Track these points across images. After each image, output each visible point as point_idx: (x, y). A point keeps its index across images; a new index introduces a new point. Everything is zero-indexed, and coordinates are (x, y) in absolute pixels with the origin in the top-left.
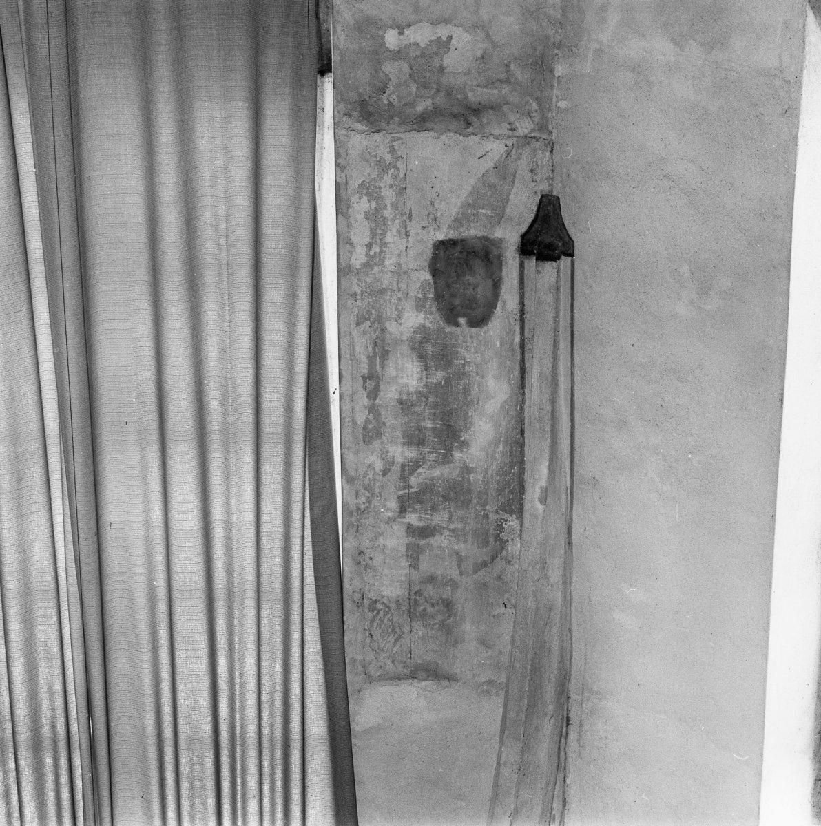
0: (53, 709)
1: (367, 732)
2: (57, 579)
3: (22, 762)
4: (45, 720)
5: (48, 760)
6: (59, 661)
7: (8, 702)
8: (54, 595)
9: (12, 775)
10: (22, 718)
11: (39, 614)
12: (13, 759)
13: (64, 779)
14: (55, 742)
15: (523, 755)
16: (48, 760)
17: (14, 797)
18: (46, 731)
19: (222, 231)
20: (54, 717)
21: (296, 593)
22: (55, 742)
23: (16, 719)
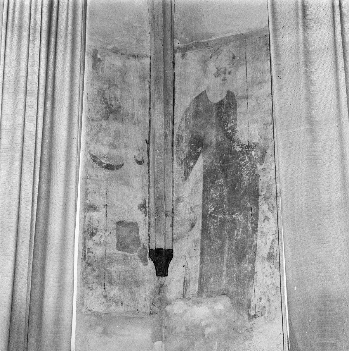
0: (12, 41)
1: (165, 247)
2: (2, 96)
3: (28, 22)
4: (15, 38)
5: (16, 20)
6: (6, 61)
7: (30, 48)
8: (24, 159)
9: (32, 17)
10: (25, 40)
11: (12, 83)
12: (31, 24)
13: (11, 11)
14: (13, 27)
15: (123, 196)
16: (16, 20)
17: (33, 8)
18: (16, 33)
19: (168, 28)
20: (12, 38)
21: (45, 165)
22: (13, 27)
23: (27, 40)
